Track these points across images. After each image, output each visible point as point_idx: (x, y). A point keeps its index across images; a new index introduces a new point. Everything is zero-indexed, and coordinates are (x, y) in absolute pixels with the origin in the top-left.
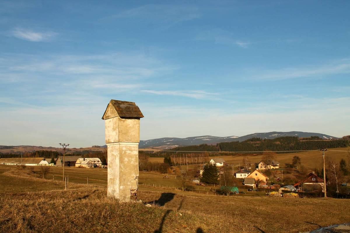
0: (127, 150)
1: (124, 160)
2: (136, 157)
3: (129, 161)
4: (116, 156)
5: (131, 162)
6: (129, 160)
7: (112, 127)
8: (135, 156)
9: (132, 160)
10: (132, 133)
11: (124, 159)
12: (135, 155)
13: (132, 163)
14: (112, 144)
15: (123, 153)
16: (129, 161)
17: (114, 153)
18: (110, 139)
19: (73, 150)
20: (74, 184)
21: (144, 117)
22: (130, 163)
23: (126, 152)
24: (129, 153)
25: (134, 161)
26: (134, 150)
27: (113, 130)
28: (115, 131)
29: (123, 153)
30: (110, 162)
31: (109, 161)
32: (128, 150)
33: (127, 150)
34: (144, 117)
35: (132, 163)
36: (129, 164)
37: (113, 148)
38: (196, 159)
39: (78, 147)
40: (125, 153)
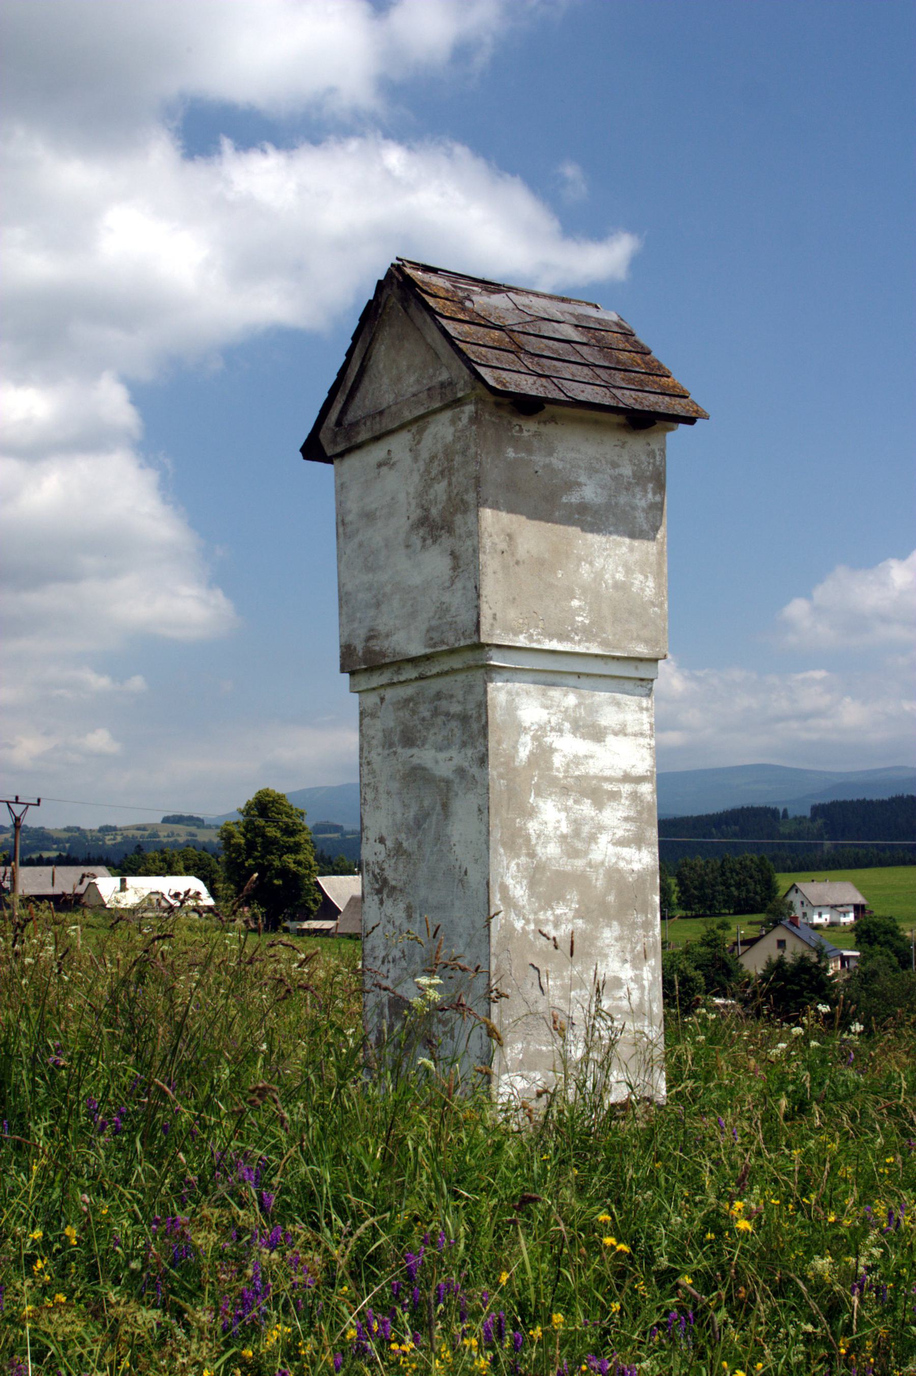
0: (561, 731)
1: (532, 826)
2: (635, 797)
3: (577, 840)
4: (448, 782)
5: (593, 838)
6: (577, 824)
7: (407, 512)
8: (626, 788)
9: (601, 828)
10: (599, 563)
11: (531, 813)
12: (627, 778)
13: (603, 850)
14: (410, 673)
15: (523, 753)
16: (577, 840)
17: (426, 756)
18: (383, 629)
19: (66, 835)
20: (431, 378)
21: (706, 417)
22: (586, 853)
23: (552, 750)
24: (577, 761)
25: (620, 833)
26: (621, 731)
27: (416, 541)
28: (447, 541)
29: (523, 753)
30: (389, 844)
31: (382, 840)
32: (567, 726)
33: (561, 731)
34: (706, 417)
35: (603, 850)
36: (579, 863)
37: (414, 712)
38: (360, 963)
39: (90, 822)
40: (542, 754)
